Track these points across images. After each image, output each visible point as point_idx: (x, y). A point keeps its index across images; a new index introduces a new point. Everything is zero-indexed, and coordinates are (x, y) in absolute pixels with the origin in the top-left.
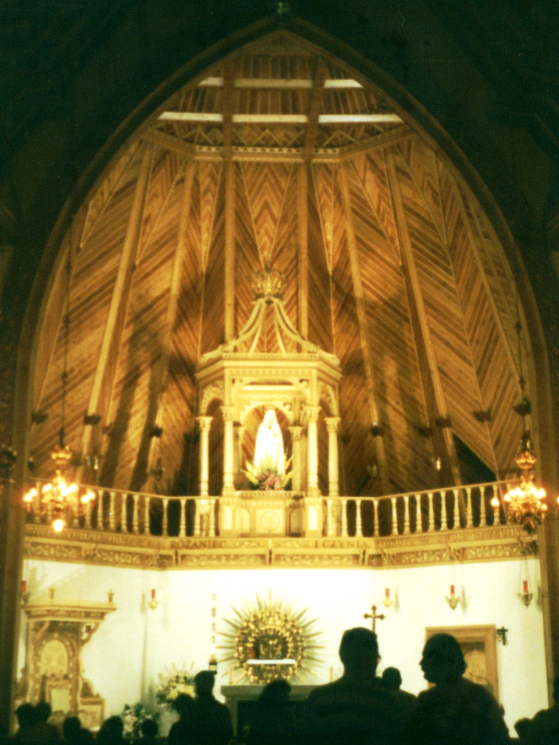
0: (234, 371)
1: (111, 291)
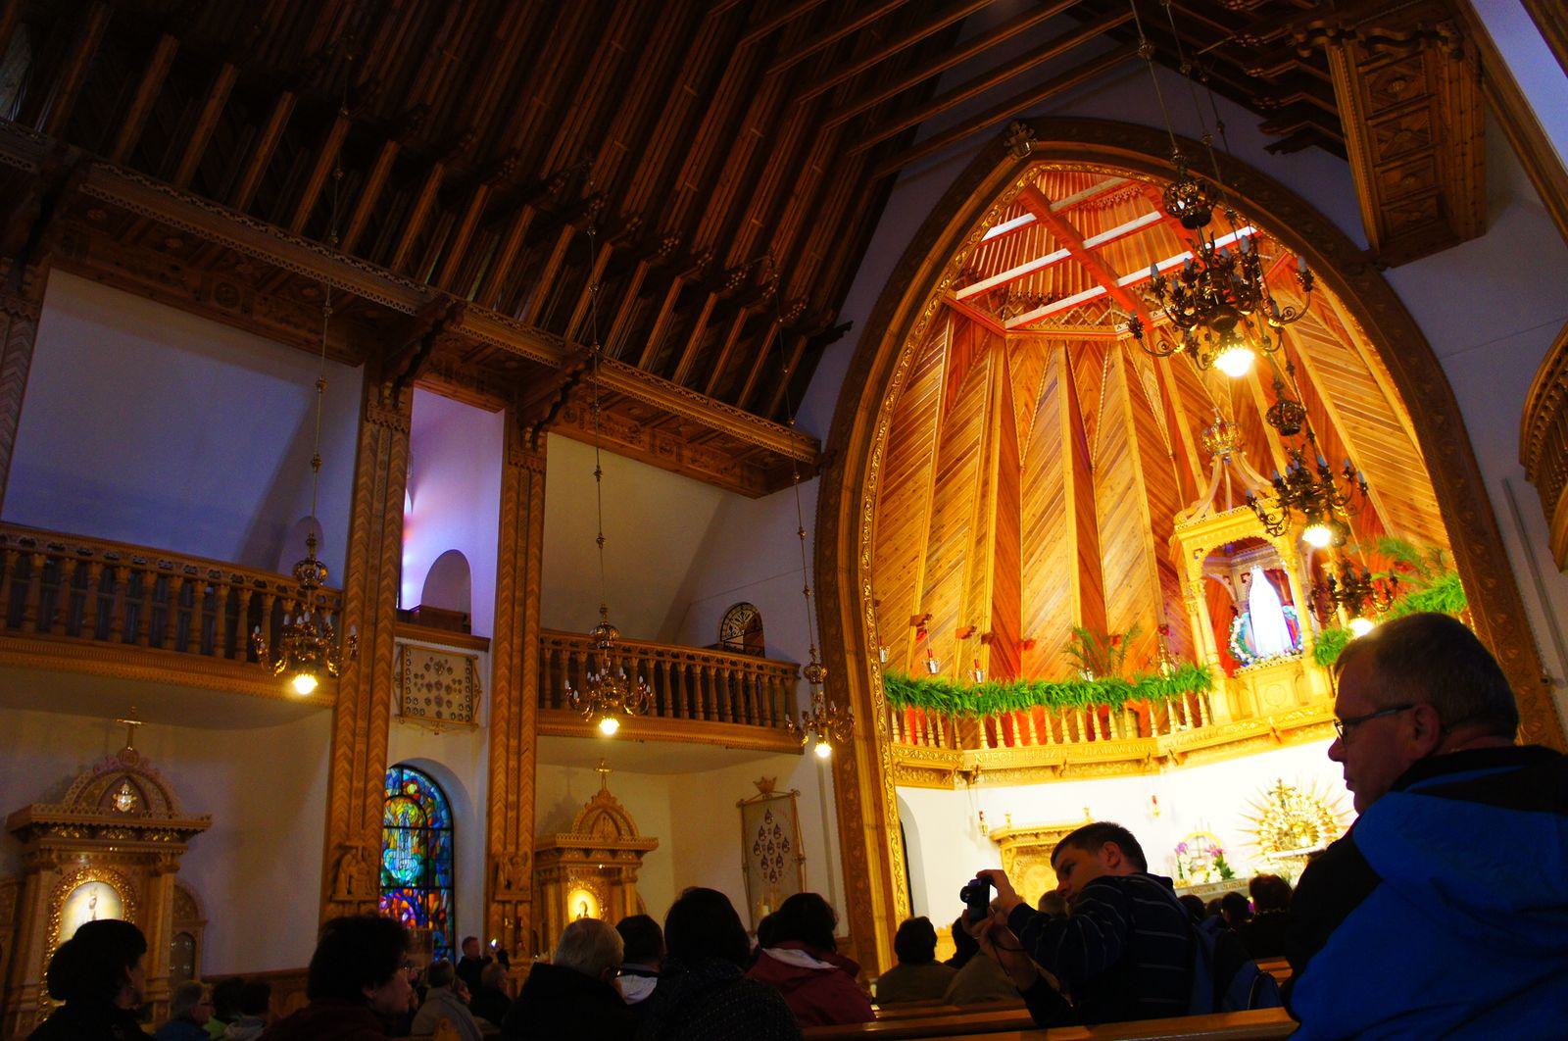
0: (1192, 541)
1: (1063, 498)
